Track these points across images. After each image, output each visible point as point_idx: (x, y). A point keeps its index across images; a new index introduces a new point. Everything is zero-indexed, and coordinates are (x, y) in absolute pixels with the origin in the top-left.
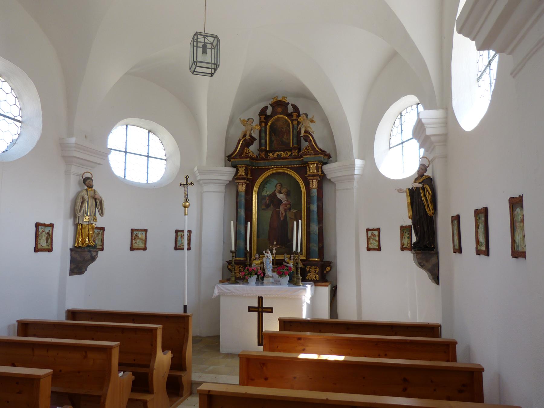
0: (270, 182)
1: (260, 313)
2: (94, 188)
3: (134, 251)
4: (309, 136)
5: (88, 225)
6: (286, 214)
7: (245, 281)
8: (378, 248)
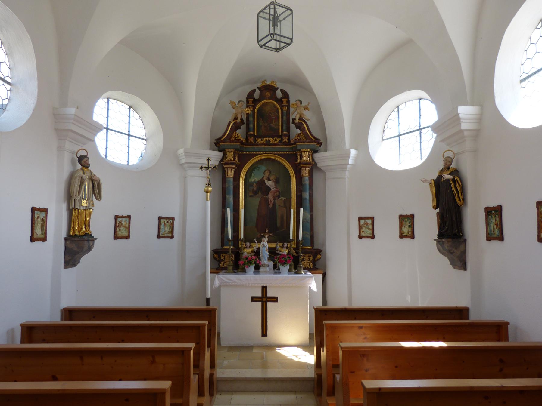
0: (258, 168)
1: (265, 303)
2: (89, 168)
3: (118, 240)
4: (303, 123)
5: (85, 210)
6: (274, 202)
7: (239, 270)
8: (371, 236)
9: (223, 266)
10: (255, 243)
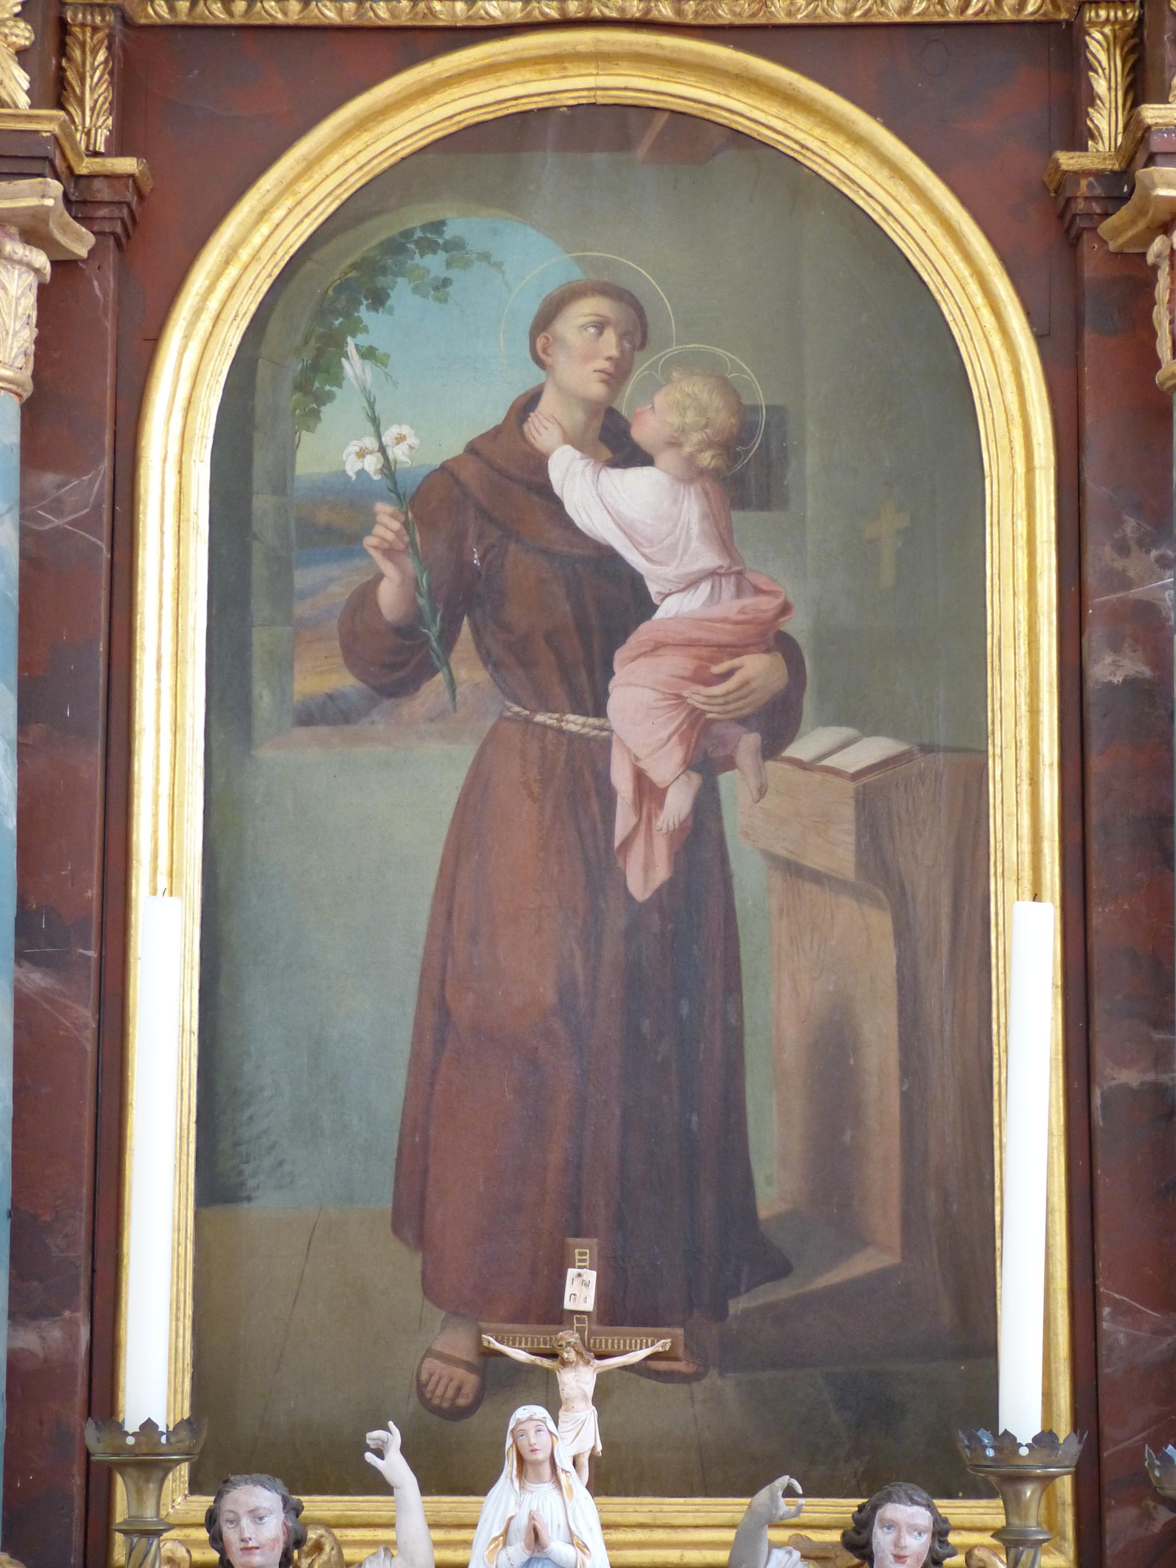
0: (434, 264)
10: (380, 1486)
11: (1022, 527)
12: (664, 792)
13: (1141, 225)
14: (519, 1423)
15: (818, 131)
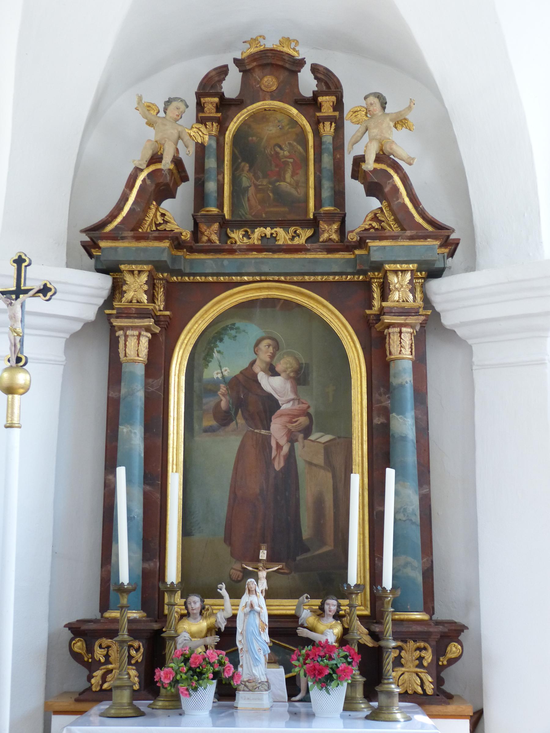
0: (233, 332)
4: (392, 172)
6: (292, 450)
7: (160, 703)
9: (101, 686)
10: (221, 597)
11: (359, 390)
12: (282, 447)
13: (383, 326)
14: (249, 582)
15: (315, 304)
